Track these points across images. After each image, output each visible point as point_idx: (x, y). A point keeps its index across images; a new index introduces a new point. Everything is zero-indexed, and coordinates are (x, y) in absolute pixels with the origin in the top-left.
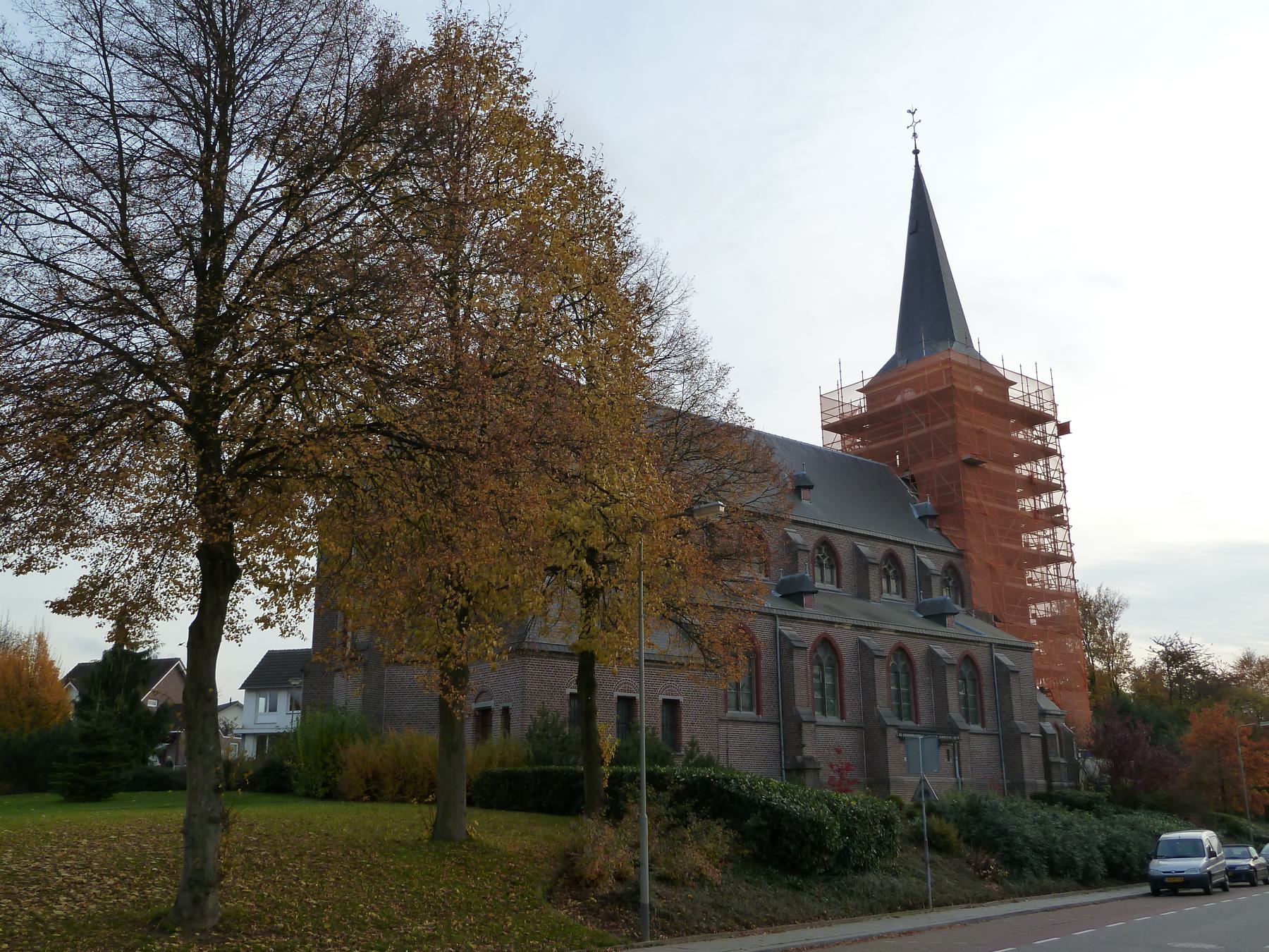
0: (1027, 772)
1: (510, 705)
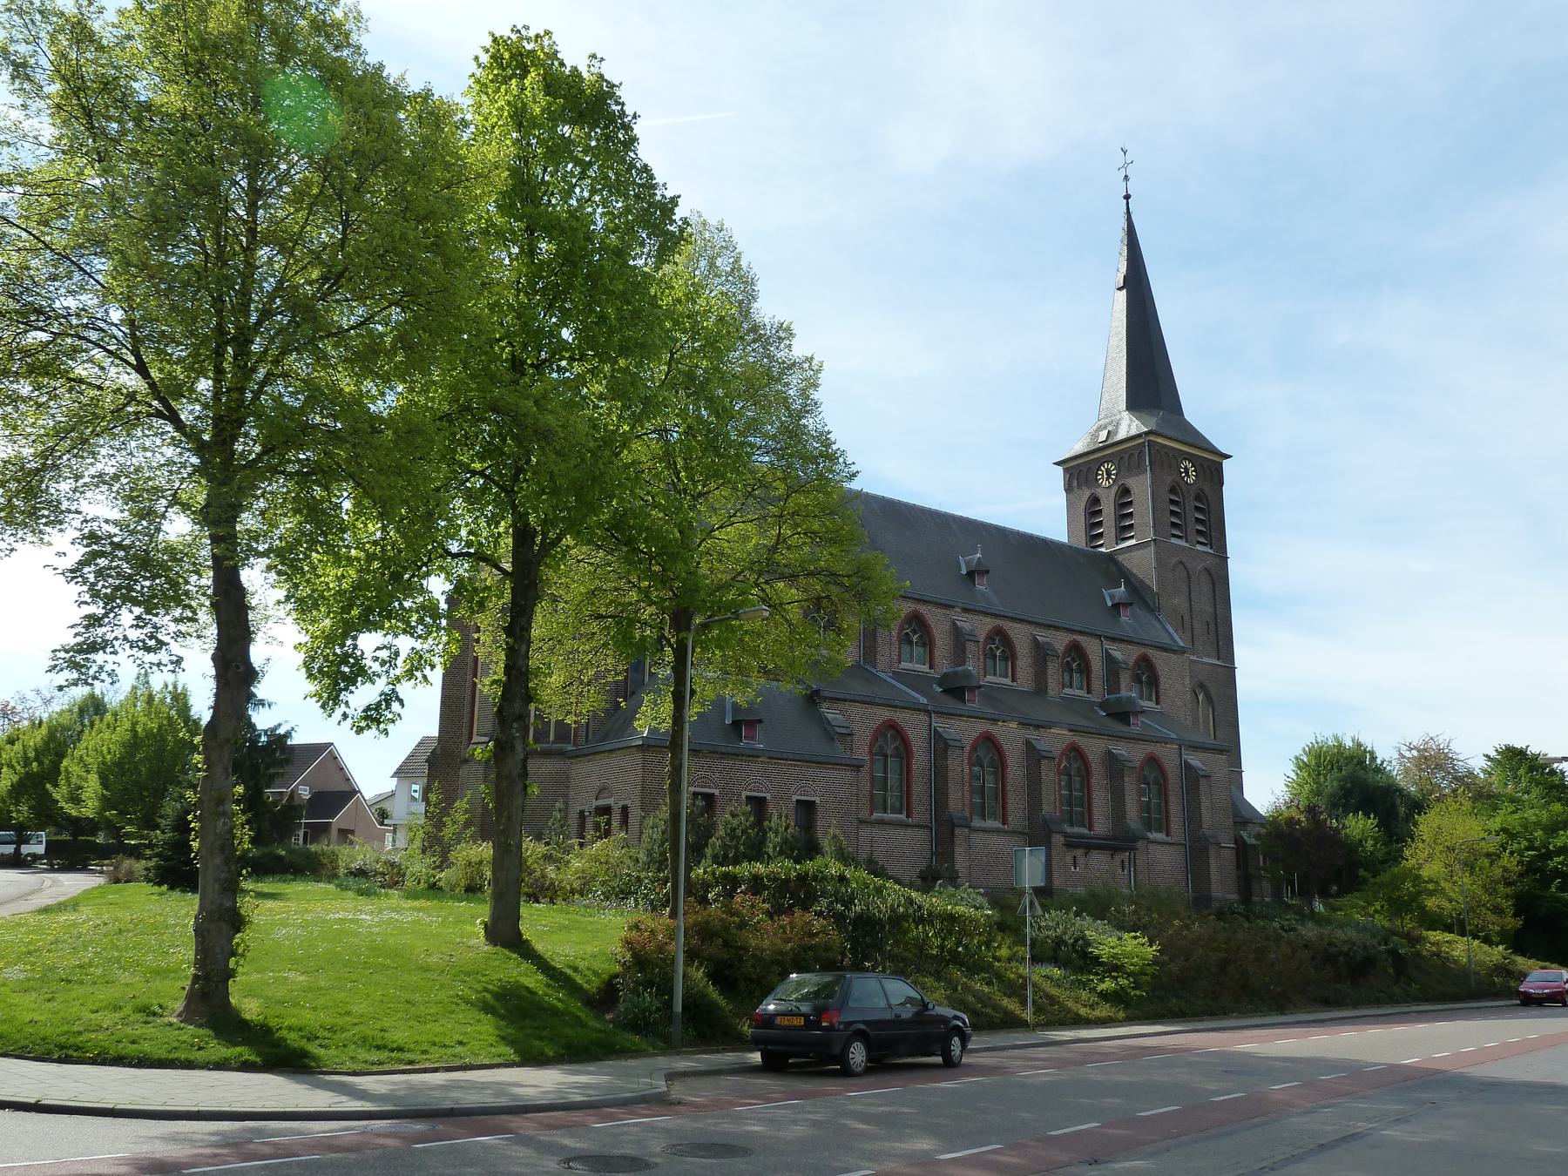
0: (1214, 886)
1: (628, 803)
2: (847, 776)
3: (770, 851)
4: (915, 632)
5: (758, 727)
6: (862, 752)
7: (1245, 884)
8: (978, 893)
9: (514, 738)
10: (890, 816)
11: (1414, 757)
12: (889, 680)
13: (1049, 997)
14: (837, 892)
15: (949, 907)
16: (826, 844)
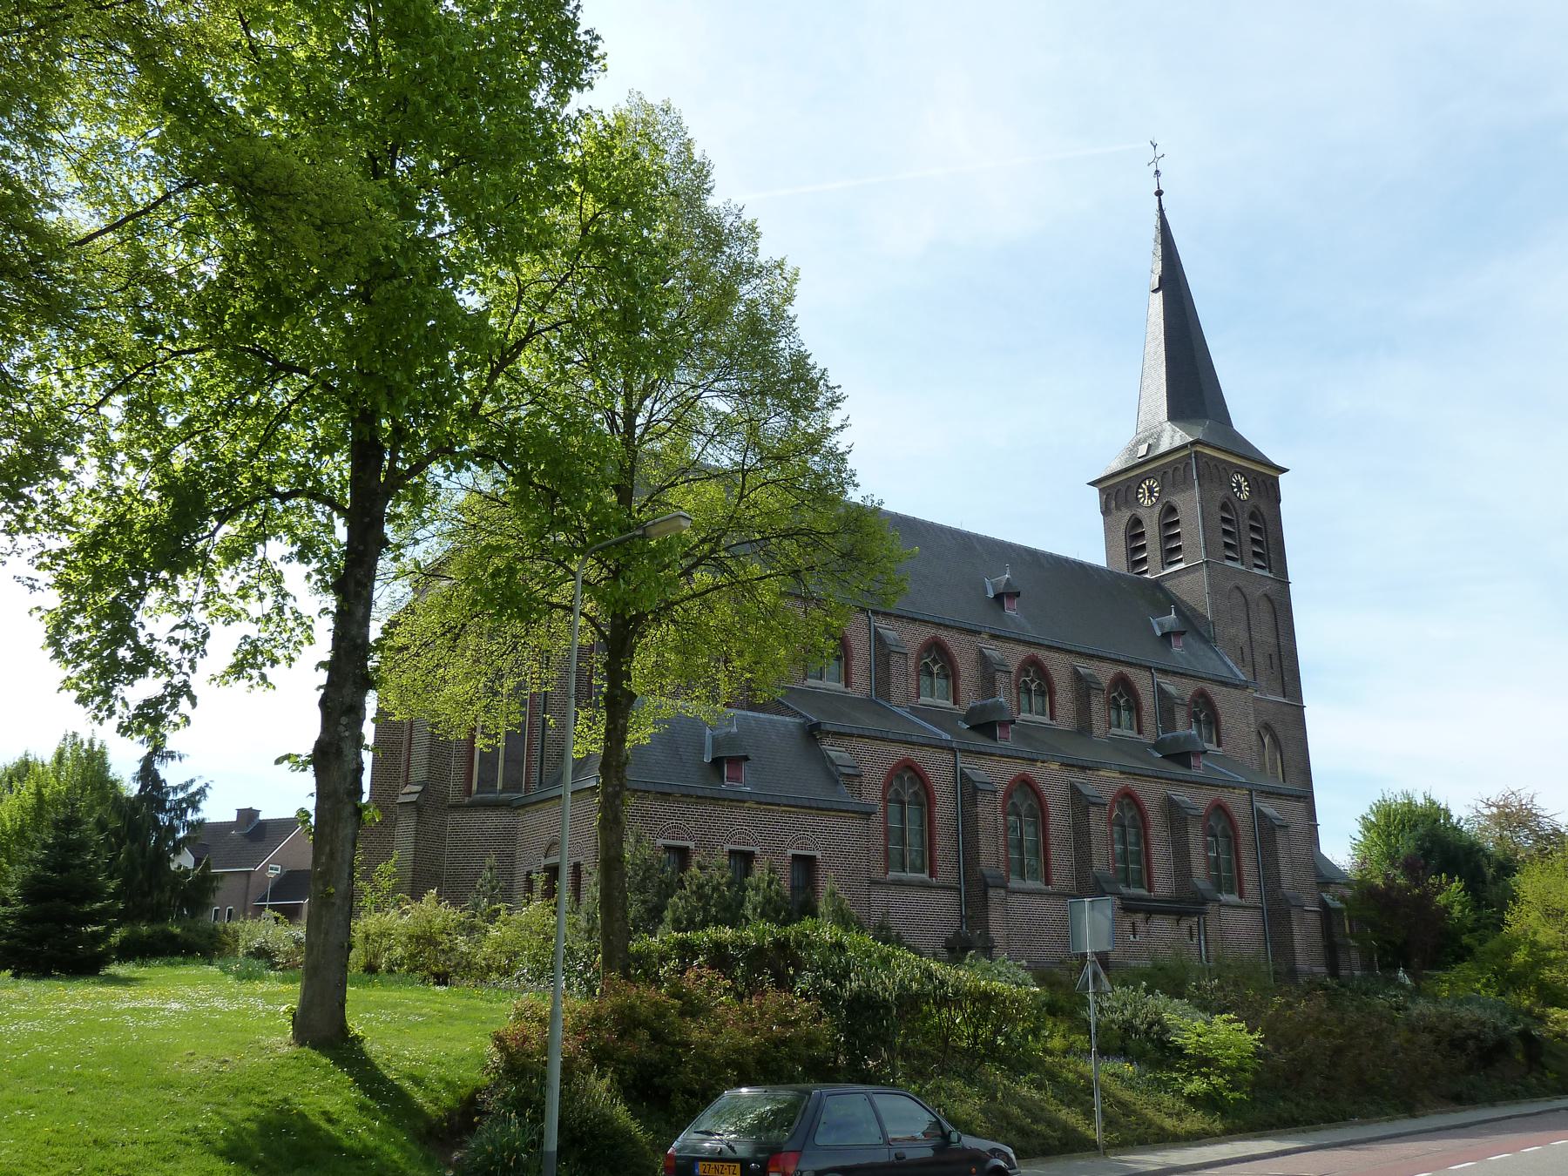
1: (580, 859)
2: (857, 824)
3: (749, 913)
4: (935, 662)
5: (744, 765)
6: (873, 795)
7: (1332, 951)
8: (1020, 966)
9: (342, 739)
10: (910, 876)
11: (1493, 814)
12: (906, 714)
13: (1122, 1104)
14: (826, 963)
15: (983, 983)
16: (823, 906)
